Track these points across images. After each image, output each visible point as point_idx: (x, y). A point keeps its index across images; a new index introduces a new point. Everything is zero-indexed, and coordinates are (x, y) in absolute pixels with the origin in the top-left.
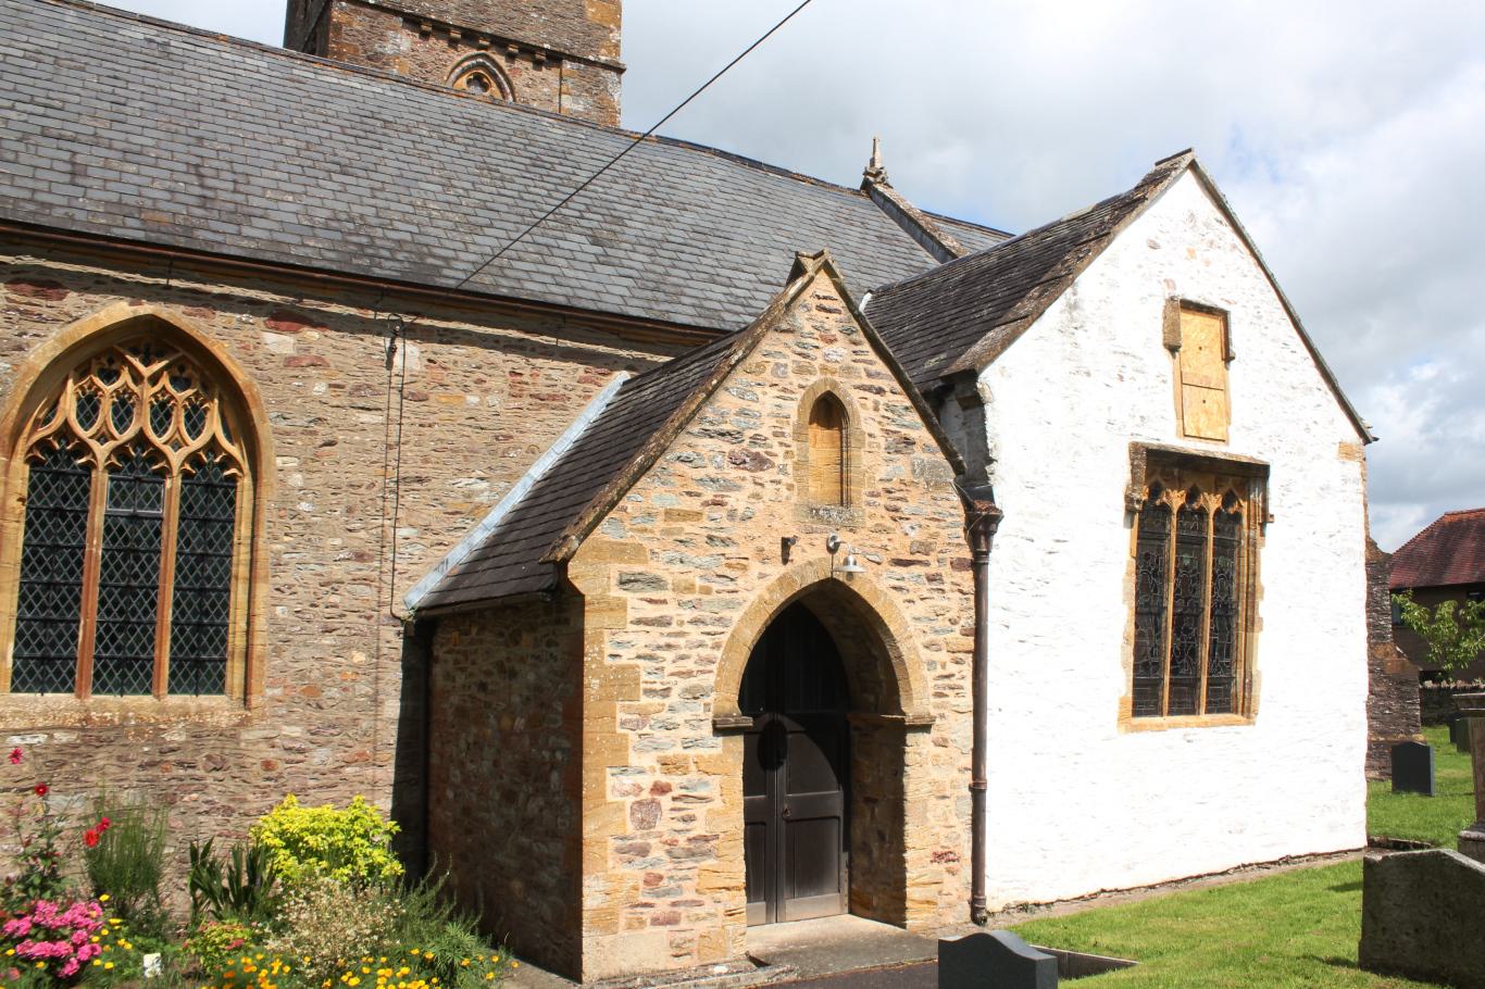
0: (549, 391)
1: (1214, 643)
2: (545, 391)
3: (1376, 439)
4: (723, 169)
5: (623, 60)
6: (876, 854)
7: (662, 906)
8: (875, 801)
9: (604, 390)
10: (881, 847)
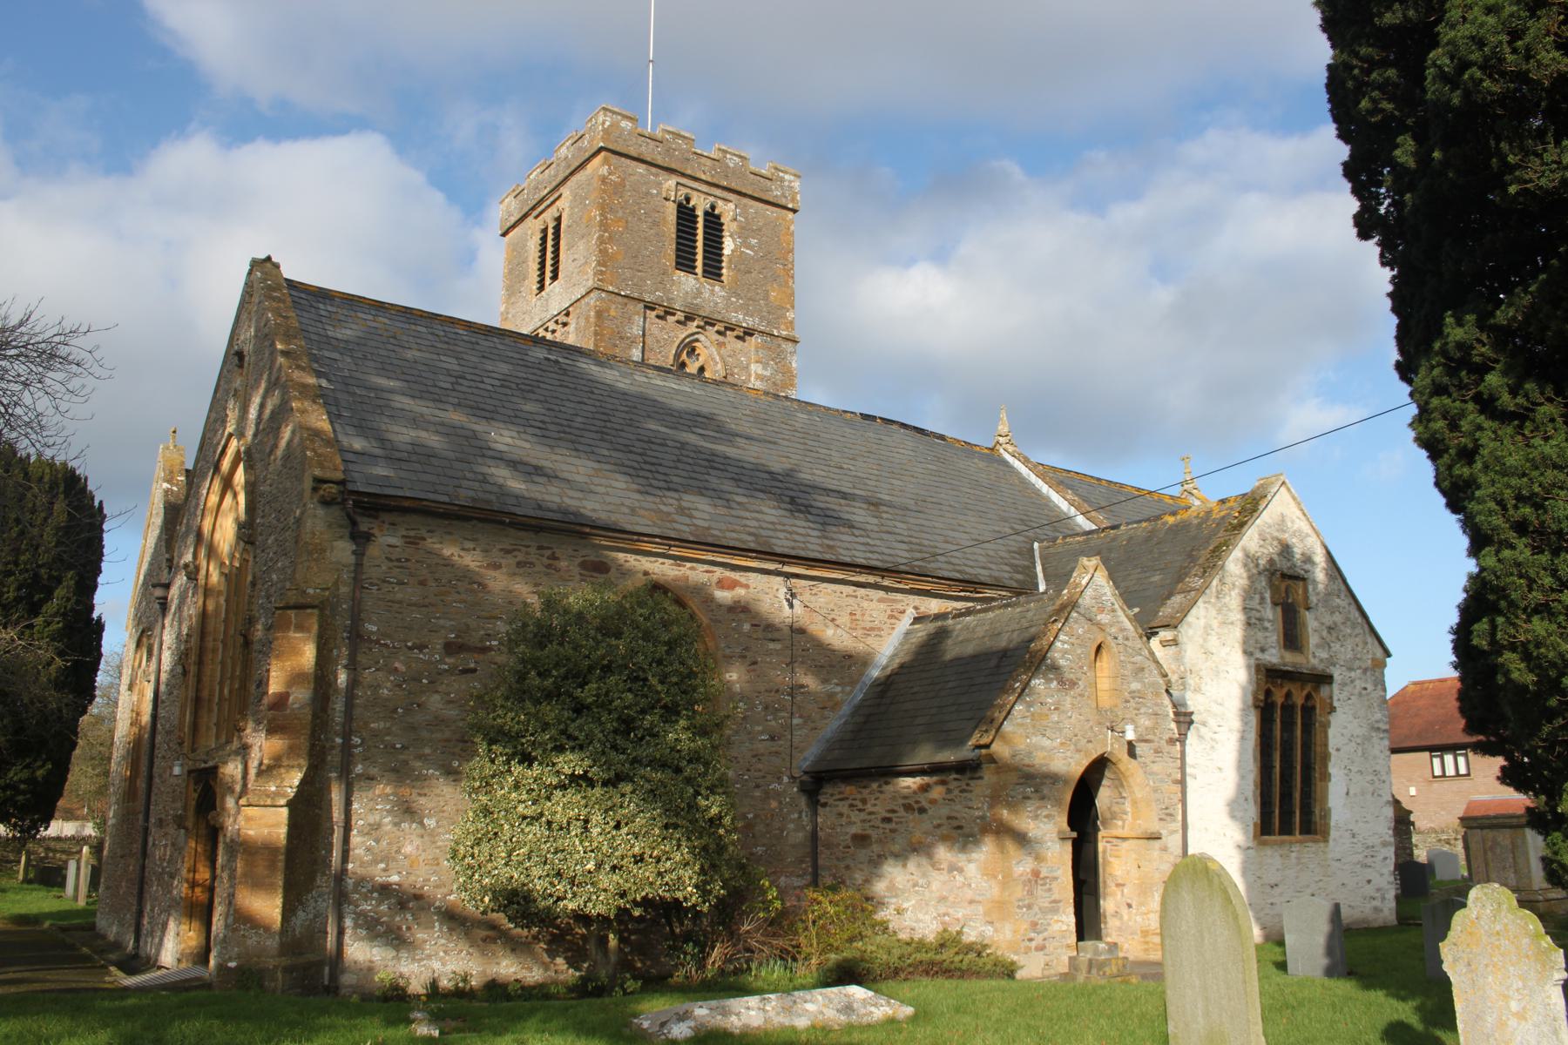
0: (872, 625)
1: (1302, 789)
2: (869, 625)
3: (98, 347)
4: (910, 440)
5: (796, 334)
6: (1126, 917)
7: (1039, 939)
8: (1123, 885)
9: (903, 622)
10: (1129, 913)
